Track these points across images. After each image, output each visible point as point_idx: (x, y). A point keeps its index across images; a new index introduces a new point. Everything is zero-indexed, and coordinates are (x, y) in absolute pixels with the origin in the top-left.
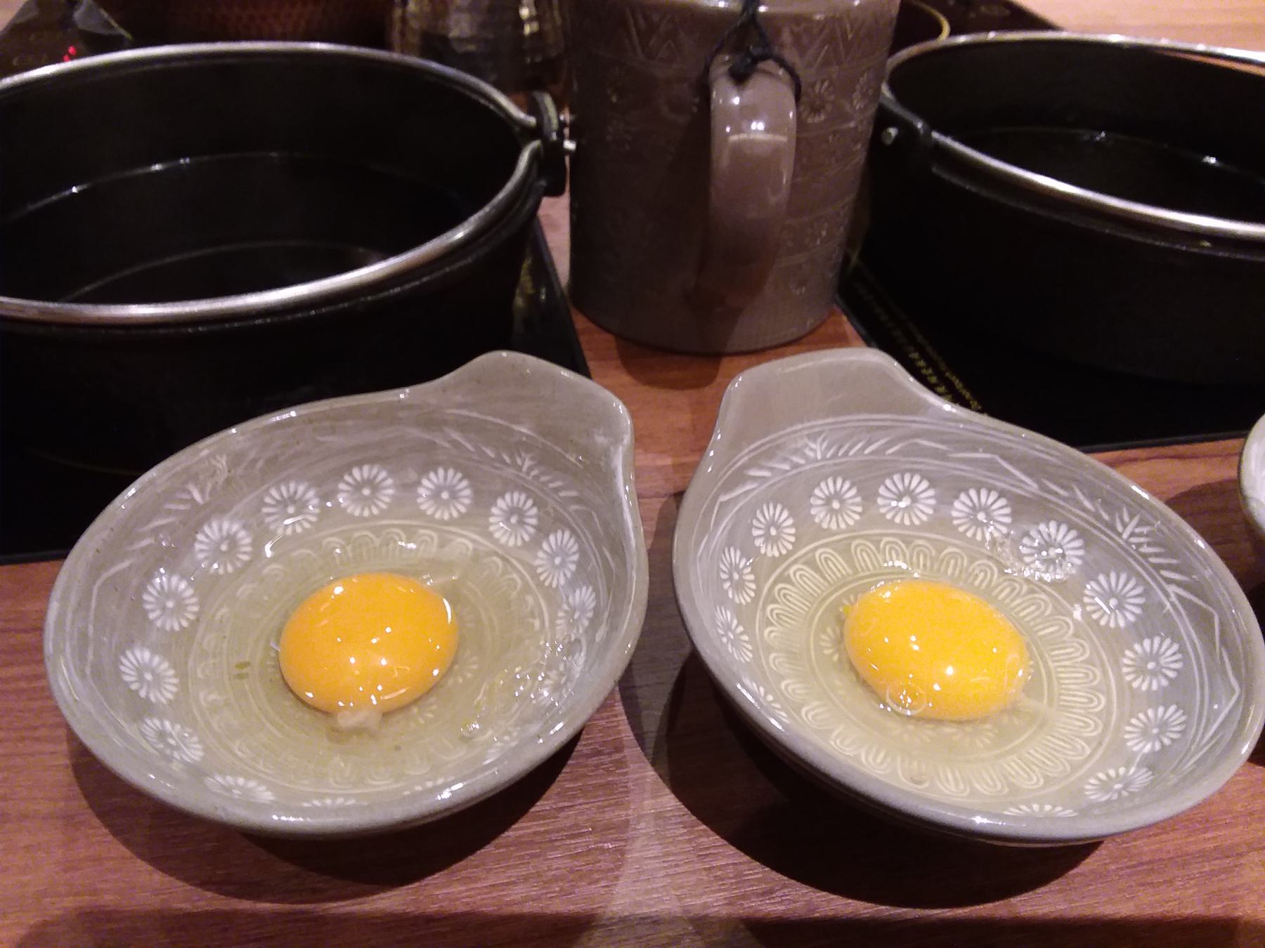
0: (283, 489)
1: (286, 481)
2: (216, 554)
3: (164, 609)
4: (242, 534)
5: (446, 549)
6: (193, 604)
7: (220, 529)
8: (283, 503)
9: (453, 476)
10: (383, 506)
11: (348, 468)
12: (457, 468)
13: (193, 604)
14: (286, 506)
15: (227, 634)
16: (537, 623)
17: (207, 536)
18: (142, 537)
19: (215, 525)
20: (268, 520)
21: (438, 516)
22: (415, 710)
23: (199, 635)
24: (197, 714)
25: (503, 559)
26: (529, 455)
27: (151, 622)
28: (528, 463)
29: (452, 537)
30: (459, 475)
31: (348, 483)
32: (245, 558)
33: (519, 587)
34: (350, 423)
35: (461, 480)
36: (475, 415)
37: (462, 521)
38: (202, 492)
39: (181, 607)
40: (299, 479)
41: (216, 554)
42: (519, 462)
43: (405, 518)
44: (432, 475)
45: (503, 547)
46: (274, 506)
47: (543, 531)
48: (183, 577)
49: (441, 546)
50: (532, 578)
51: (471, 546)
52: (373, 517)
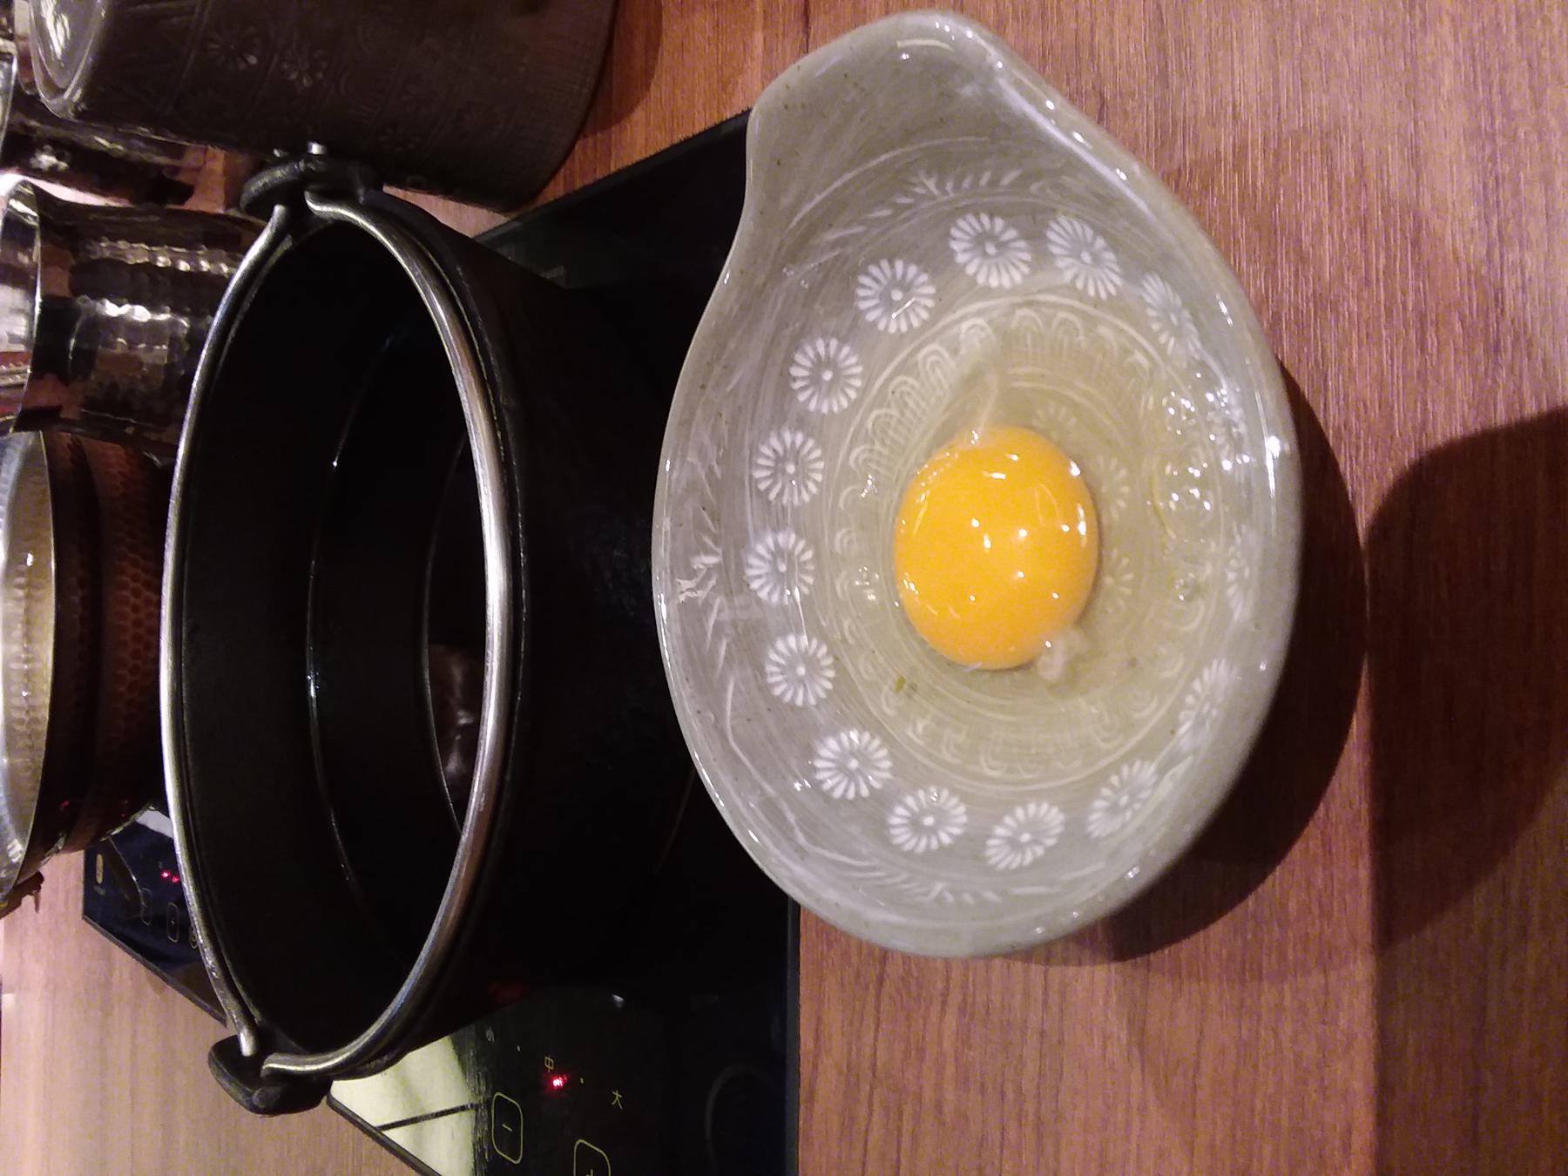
0: (762, 461)
1: (754, 451)
2: (782, 581)
3: (801, 681)
4: (781, 538)
5: (963, 352)
6: (818, 648)
7: (761, 557)
8: (777, 471)
9: (881, 271)
10: (859, 370)
11: (786, 378)
12: (875, 260)
13: (818, 648)
14: (784, 472)
15: (872, 646)
16: (1139, 357)
17: (759, 577)
18: (714, 652)
19: (753, 561)
20: (785, 500)
21: (916, 323)
22: (1108, 580)
23: (851, 669)
24: (927, 762)
25: (1030, 304)
26: (922, 173)
27: (805, 707)
28: (931, 184)
29: (955, 331)
30: (885, 264)
31: (803, 389)
32: (809, 555)
33: (1079, 325)
34: (732, 345)
35: (892, 266)
36: (818, 198)
37: (944, 304)
38: (708, 552)
39: (811, 661)
40: (763, 437)
41: (782, 581)
42: (919, 190)
43: (890, 360)
44: (861, 292)
45: (1014, 291)
46: (775, 483)
47: (1035, 236)
48: (783, 634)
49: (955, 352)
50: (1081, 300)
51: (980, 321)
52: (863, 392)
